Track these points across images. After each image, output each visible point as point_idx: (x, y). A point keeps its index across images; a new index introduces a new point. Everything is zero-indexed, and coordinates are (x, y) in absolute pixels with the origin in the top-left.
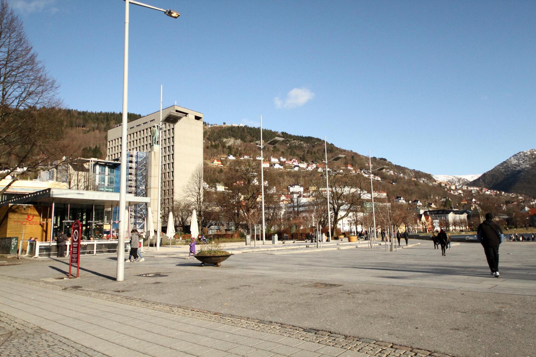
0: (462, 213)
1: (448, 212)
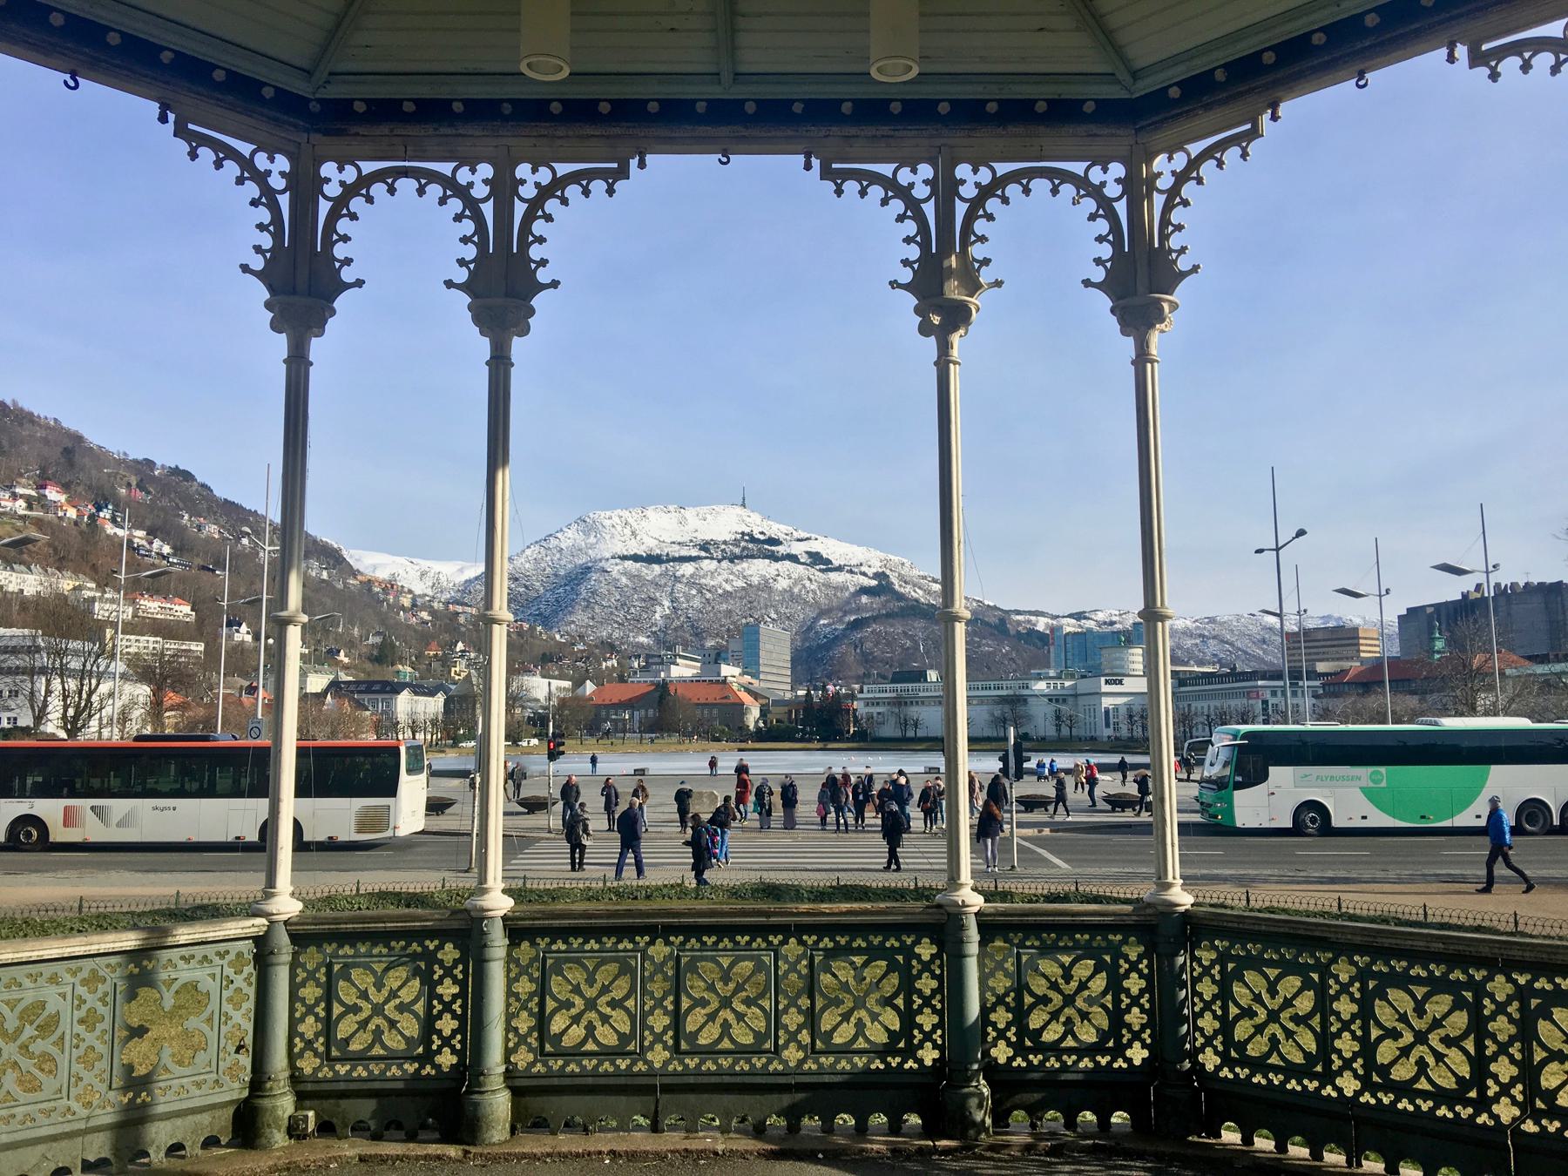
0: (432, 694)
1: (396, 689)
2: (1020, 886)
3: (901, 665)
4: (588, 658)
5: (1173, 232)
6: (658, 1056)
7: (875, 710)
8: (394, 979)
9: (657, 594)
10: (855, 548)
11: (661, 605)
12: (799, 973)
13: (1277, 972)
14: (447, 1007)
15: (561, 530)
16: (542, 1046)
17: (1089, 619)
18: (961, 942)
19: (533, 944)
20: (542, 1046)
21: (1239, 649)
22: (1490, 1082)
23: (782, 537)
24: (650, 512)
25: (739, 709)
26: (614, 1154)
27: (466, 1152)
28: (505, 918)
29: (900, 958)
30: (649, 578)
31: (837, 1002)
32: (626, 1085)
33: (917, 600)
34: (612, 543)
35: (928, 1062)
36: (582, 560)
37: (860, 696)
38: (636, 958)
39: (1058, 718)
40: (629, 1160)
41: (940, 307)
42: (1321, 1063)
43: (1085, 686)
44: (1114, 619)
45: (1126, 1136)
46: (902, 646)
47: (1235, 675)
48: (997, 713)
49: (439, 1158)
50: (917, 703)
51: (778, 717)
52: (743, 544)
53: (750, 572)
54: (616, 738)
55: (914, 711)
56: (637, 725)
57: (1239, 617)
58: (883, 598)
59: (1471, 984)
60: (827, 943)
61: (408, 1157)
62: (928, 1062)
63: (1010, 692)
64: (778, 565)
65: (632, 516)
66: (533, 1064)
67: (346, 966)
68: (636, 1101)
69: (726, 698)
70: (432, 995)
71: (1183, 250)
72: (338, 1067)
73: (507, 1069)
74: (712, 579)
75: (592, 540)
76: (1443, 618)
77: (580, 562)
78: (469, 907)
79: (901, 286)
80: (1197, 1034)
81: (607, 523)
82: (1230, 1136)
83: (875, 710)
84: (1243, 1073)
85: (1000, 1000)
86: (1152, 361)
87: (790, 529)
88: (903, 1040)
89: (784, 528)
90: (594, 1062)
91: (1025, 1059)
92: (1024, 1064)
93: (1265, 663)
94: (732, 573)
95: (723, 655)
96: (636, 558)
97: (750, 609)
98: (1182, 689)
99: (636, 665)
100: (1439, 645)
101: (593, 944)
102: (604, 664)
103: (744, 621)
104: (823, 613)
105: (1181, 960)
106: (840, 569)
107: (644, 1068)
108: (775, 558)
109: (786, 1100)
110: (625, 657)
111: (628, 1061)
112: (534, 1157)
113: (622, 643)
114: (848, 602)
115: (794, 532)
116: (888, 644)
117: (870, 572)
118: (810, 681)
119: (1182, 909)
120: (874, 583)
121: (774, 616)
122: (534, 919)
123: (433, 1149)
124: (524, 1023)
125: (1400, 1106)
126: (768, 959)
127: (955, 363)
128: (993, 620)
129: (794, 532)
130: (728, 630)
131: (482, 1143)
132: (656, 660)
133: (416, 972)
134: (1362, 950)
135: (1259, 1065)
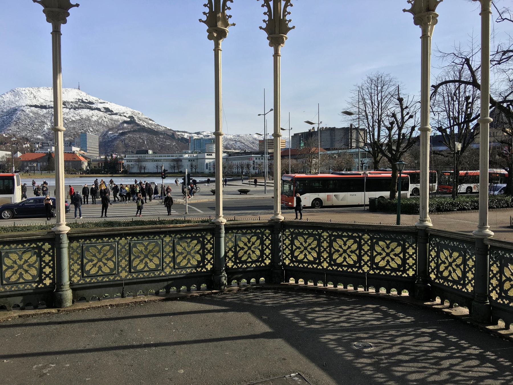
2: (192, 218)
3: (139, 148)
4: (17, 143)
5: (287, 14)
6: (124, 274)
7: (130, 163)
8: (26, 256)
9: (45, 120)
10: (122, 107)
11: (47, 124)
12: (126, 249)
13: (307, 236)
14: (47, 264)
15: (4, 94)
16: (83, 274)
17: (201, 134)
18: (220, 233)
19: (126, 239)
20: (83, 274)
21: (246, 145)
22: (362, 262)
23: (94, 101)
24: (41, 89)
25: (80, 163)
26: (111, 305)
27: (59, 311)
28: (68, 234)
29: (201, 239)
30: (41, 114)
31: (138, 257)
32: (113, 284)
33: (144, 126)
34: (26, 100)
35: (267, 264)
36: (13, 106)
37: (125, 158)
38: (115, 244)
39: (192, 166)
40: (117, 307)
41: (217, 30)
42: (318, 260)
43: (200, 156)
44: (209, 134)
45: (264, 284)
46: (139, 142)
47: (245, 153)
48: (172, 164)
49: (49, 313)
50: (145, 161)
51: (95, 165)
52: (79, 103)
53: (82, 114)
54: (31, 173)
55: (144, 164)
56: (39, 169)
57: (246, 135)
58: (132, 125)
59: (359, 237)
60: (178, 236)
61: (37, 314)
62: (267, 264)
63: (176, 158)
64: (93, 112)
65: (34, 91)
66: (80, 280)
67: (7, 253)
68: (116, 289)
69: (74, 159)
70: (41, 261)
71: (290, 21)
72: (177, 271)
73: (70, 283)
74: (67, 115)
75: (17, 98)
76: (304, 137)
77: (13, 107)
78: (54, 230)
79: (203, 21)
80: (284, 255)
81: (23, 92)
82: (292, 281)
83: (130, 163)
84: (296, 264)
85: (230, 249)
86: (279, 56)
87: (97, 99)
88: (202, 263)
89: (95, 98)
90: (102, 278)
91: (237, 265)
92: (236, 267)
93: (253, 149)
94: (75, 114)
95: (73, 143)
96: (36, 106)
97: (82, 127)
98: (230, 157)
99: (37, 146)
100: (302, 145)
101: (100, 241)
102: (24, 146)
103: (80, 131)
104: (110, 129)
105: (280, 235)
106: (116, 114)
107: (119, 279)
108: (91, 109)
109: (166, 284)
110: (33, 143)
111: (113, 277)
112: (84, 310)
113: (31, 138)
114: (119, 126)
115: (99, 100)
116: (134, 141)
117: (127, 116)
118: (106, 153)
119: (281, 221)
120: (129, 119)
121: (92, 130)
122: (78, 234)
123: (46, 311)
124: (76, 267)
125: (338, 269)
126: (160, 242)
127: (221, 50)
128: (170, 134)
129: (99, 100)
130: (74, 134)
131: (64, 307)
132: (46, 144)
133: (35, 253)
134: (330, 229)
135: (301, 262)
